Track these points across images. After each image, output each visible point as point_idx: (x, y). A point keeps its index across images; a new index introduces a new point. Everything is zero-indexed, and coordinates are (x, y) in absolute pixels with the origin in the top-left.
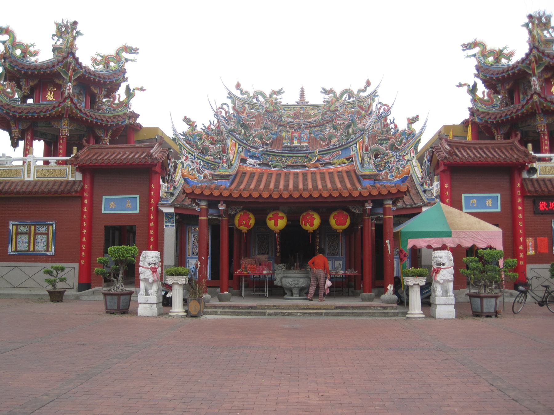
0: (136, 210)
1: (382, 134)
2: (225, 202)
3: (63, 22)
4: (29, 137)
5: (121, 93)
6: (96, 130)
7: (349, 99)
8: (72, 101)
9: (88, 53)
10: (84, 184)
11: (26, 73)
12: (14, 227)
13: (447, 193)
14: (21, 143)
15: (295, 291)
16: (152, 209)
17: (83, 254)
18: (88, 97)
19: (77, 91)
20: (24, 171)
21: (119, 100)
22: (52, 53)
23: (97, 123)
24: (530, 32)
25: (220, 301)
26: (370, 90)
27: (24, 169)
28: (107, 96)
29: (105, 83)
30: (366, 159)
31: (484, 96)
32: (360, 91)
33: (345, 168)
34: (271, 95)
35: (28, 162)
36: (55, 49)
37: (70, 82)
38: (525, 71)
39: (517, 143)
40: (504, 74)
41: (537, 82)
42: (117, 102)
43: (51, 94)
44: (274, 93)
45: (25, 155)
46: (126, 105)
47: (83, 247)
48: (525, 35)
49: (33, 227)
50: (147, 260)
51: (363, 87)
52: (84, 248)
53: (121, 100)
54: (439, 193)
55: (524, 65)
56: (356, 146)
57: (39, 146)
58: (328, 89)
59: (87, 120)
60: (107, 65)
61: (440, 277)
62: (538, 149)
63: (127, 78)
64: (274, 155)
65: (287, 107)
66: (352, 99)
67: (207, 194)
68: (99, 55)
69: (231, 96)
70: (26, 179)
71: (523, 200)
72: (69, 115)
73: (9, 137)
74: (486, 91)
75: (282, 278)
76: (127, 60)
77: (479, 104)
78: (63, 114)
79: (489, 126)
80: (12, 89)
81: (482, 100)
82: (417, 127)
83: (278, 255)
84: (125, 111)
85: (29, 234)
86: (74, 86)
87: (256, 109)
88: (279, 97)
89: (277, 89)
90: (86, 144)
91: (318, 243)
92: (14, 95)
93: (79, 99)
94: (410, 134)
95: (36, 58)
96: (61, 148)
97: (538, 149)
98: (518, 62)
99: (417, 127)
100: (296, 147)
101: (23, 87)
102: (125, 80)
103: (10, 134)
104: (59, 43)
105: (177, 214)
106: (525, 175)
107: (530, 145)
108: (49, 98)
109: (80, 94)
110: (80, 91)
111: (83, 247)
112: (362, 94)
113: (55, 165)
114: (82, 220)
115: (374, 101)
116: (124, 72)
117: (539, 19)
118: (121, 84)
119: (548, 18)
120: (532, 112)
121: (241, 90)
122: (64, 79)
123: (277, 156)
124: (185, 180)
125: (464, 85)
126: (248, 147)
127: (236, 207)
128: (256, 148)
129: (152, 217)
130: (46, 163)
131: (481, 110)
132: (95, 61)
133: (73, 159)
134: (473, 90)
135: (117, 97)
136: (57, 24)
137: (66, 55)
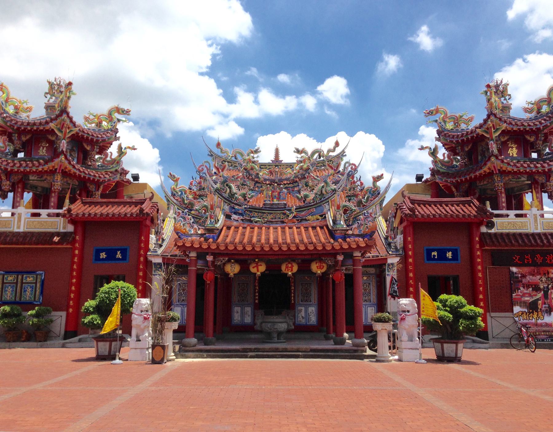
1: (350, 191)
3: (55, 80)
4: (20, 190)
5: (113, 150)
6: (88, 185)
7: (320, 158)
8: (66, 158)
10: (76, 236)
11: (18, 128)
13: (410, 246)
15: (275, 335)
16: (142, 259)
17: (71, 302)
18: (80, 153)
19: (70, 147)
20: (14, 222)
22: (45, 110)
23: (89, 178)
25: (205, 345)
26: (338, 150)
28: (99, 153)
29: (97, 141)
30: (338, 216)
33: (318, 224)
35: (19, 214)
36: (49, 107)
37: (64, 139)
38: (483, 135)
40: (463, 138)
42: (108, 159)
43: (43, 149)
46: (118, 162)
47: (72, 296)
49: (20, 277)
50: (140, 307)
51: (332, 147)
52: (72, 297)
53: (113, 157)
54: (402, 245)
56: (329, 204)
58: (300, 149)
59: (80, 176)
60: (99, 124)
62: (495, 206)
63: (119, 137)
64: (256, 212)
65: (263, 166)
66: (322, 159)
67: (196, 247)
68: (91, 114)
70: (16, 230)
71: (482, 253)
72: (62, 170)
74: (447, 153)
75: (261, 323)
76: (119, 121)
77: (440, 165)
78: (56, 169)
79: (449, 184)
81: (442, 162)
82: (381, 184)
83: (257, 301)
84: (117, 168)
86: (67, 142)
87: (235, 166)
88: (255, 156)
90: (79, 197)
96: (53, 200)
97: (495, 206)
99: (381, 184)
100: (276, 204)
101: (15, 142)
102: (117, 139)
106: (484, 229)
107: (488, 203)
108: (41, 153)
109: (72, 150)
110: (72, 147)
111: (72, 296)
112: (331, 154)
113: (47, 217)
114: (72, 270)
115: (342, 159)
116: (116, 131)
118: (113, 143)
120: (489, 173)
122: (57, 135)
123: (258, 212)
125: (426, 148)
126: (232, 205)
127: (222, 259)
128: (240, 206)
129: (141, 267)
131: (441, 170)
132: (86, 119)
133: (66, 212)
134: (433, 153)
135: (110, 154)
136: (49, 83)
137: (60, 112)
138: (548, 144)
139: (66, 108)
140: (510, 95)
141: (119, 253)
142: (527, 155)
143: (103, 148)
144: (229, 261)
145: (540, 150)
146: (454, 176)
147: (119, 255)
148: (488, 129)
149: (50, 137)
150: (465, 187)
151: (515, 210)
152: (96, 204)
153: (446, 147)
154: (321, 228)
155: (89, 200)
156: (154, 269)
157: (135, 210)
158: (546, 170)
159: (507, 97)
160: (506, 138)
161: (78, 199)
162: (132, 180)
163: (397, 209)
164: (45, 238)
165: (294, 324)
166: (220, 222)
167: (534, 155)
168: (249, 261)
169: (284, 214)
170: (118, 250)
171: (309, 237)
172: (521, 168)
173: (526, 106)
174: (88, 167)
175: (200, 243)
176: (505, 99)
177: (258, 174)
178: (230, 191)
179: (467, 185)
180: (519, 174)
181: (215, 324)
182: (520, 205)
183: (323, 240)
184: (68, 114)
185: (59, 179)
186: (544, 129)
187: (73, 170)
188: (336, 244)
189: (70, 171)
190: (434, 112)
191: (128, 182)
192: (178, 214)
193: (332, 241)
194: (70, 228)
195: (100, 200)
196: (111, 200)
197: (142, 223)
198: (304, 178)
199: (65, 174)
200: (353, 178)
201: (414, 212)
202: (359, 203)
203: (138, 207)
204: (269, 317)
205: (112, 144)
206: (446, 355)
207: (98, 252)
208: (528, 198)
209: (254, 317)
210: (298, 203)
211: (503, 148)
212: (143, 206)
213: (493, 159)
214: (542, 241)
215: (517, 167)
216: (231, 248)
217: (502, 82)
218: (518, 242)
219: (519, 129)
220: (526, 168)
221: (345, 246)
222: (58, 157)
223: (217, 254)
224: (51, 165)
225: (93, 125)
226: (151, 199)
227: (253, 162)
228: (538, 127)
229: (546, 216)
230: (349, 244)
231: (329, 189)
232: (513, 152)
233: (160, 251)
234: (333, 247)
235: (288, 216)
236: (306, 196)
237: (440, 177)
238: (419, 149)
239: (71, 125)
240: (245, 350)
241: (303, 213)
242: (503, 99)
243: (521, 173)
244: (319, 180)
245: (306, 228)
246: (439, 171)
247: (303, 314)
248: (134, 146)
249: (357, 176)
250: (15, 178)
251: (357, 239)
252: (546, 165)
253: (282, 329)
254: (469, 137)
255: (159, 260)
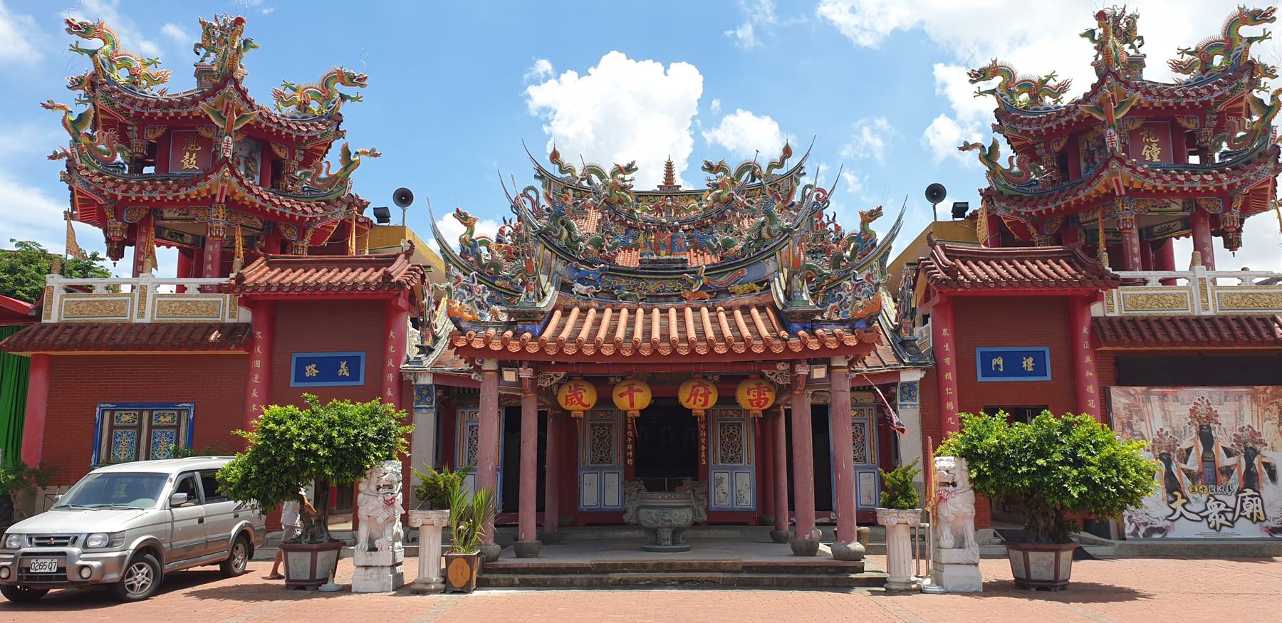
0: (983, 376)
2: (531, 364)
5: (332, 162)
6: (282, 228)
7: (753, 180)
8: (233, 173)
9: (266, 85)
12: (107, 415)
14: (129, 251)
15: (667, 535)
19: (245, 153)
20: (132, 304)
21: (327, 172)
24: (1101, 46)
25: (518, 556)
26: (791, 163)
27: (133, 300)
28: (305, 164)
29: (300, 138)
31: (1012, 165)
32: (772, 166)
34: (613, 175)
36: (201, 73)
38: (1091, 117)
39: (1078, 250)
41: (1116, 138)
42: (323, 175)
44: (620, 170)
45: (136, 273)
48: (1088, 51)
49: (146, 415)
53: (333, 172)
55: (1090, 105)
57: (168, 258)
58: (715, 163)
60: (303, 107)
61: (947, 510)
65: (641, 196)
66: (757, 181)
67: (496, 348)
68: (287, 86)
69: (541, 174)
70: (136, 320)
73: (104, 239)
75: (638, 509)
76: (343, 98)
78: (214, 196)
79: (1023, 220)
80: (109, 144)
81: (1007, 173)
82: (879, 230)
83: (630, 461)
85: (139, 427)
88: (628, 177)
89: (624, 164)
91: (703, 440)
92: (114, 156)
93: (247, 168)
94: (864, 240)
95: (161, 87)
98: (1077, 102)
101: (134, 141)
103: (105, 232)
104: (208, 61)
105: (438, 387)
108: (186, 165)
109: (249, 159)
110: (251, 152)
112: (775, 171)
115: (798, 182)
117: (1117, 19)
119: (1133, 20)
121: (561, 165)
124: (456, 322)
125: (975, 145)
128: (590, 265)
130: (181, 289)
132: (279, 96)
134: (989, 156)
135: (325, 165)
137: (220, 81)
138: (1227, 134)
139: (232, 71)
140: (1141, 38)
141: (343, 365)
142: (1180, 159)
143: (313, 155)
144: (569, 378)
145: (1206, 149)
146: (1032, 201)
147: (344, 370)
148: (1101, 104)
149: (204, 133)
150: (1054, 226)
151: (1155, 270)
152: (295, 265)
153: (1015, 144)
154: (761, 309)
155: (281, 257)
156: (416, 398)
157: (374, 276)
158: (1225, 187)
159: (1137, 43)
160: (1137, 125)
161: (259, 257)
162: (375, 220)
163: (917, 271)
164: (192, 335)
165: (707, 510)
166: (548, 298)
167: (1194, 160)
168: (612, 380)
169: (683, 281)
170: (343, 359)
171: (735, 327)
172: (1173, 183)
173: (1178, 58)
174: (286, 193)
175: (505, 343)
176: (1132, 47)
177: (632, 211)
178: (570, 234)
179: (1059, 221)
180: (1166, 196)
181: (540, 508)
182: (1164, 261)
183: (764, 332)
184: (237, 83)
185: (221, 216)
186: (1217, 104)
187: (249, 198)
188: (794, 340)
189: (242, 199)
190: (989, 74)
191: (368, 222)
192: (454, 280)
193: (783, 333)
194: (245, 315)
195: (306, 256)
196: (326, 257)
197: (388, 304)
198: (724, 218)
199: (233, 205)
200: (821, 216)
201: (955, 277)
202: (837, 261)
203: (381, 272)
204: (656, 495)
205: (330, 147)
206: (1034, 576)
207: (302, 364)
208: (1182, 249)
209: (624, 495)
210: (710, 259)
211: (1133, 140)
212: (390, 269)
213: (1114, 165)
214: (1219, 333)
215: (1165, 182)
216: (570, 350)
217: (1124, 11)
218: (1168, 334)
219: (1164, 104)
220: (1182, 182)
221: (814, 345)
222: (217, 169)
223: (540, 364)
224: (203, 186)
225: (293, 108)
226: (408, 254)
227: (623, 188)
228: (1206, 99)
229: (1221, 282)
230: (822, 340)
231: (775, 227)
232: (1153, 152)
233: (428, 361)
234: (787, 347)
235: (691, 285)
236: (728, 244)
237: (1004, 204)
238: (960, 149)
239: (244, 106)
240: (602, 569)
241: (722, 279)
242: (1127, 46)
243: (1171, 194)
244: (754, 210)
245: (730, 311)
246: (1001, 193)
247: (725, 486)
248: (373, 150)
249: (829, 212)
250: (131, 216)
251: (838, 330)
252: (1224, 177)
253: (682, 523)
254: (1063, 121)
255: (427, 380)
